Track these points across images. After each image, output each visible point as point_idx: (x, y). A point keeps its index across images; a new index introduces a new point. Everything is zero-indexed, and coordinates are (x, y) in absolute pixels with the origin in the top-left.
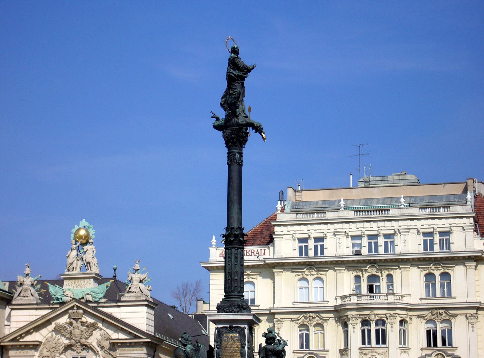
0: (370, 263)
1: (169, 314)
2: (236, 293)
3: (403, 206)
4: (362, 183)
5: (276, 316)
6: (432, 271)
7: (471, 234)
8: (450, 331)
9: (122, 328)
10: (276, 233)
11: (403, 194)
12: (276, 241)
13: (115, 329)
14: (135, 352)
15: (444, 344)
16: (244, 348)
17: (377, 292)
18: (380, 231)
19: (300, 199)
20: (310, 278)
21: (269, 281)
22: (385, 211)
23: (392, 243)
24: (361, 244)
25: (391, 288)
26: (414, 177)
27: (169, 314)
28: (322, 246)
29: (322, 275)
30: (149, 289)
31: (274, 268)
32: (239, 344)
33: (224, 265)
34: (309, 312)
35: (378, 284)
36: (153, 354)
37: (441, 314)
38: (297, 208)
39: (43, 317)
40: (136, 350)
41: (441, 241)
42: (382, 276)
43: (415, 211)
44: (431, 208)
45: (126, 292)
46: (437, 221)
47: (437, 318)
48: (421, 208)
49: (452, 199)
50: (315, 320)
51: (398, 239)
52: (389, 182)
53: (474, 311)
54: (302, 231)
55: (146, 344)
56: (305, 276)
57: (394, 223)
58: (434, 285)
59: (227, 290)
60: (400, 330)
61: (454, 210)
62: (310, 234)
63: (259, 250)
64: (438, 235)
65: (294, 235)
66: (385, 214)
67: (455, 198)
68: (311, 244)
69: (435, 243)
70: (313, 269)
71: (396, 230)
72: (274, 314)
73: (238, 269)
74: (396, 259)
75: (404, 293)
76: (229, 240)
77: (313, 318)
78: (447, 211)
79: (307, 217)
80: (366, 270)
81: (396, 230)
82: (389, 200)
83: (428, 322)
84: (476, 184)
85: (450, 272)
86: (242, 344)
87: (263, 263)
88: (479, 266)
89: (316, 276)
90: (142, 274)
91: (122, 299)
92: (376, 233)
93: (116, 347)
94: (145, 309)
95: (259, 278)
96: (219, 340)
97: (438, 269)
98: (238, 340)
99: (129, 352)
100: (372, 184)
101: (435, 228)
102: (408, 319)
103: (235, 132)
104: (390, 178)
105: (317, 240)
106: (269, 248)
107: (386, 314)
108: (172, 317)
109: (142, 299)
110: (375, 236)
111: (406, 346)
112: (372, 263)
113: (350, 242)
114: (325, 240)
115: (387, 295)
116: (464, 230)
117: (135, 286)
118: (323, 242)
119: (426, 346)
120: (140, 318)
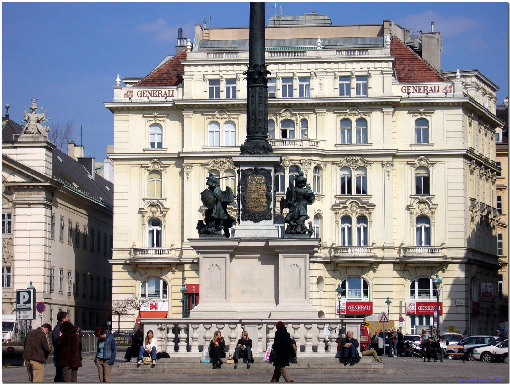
0: (285, 108)
1: (58, 157)
2: (260, 134)
3: (319, 48)
4: (272, 23)
5: (185, 161)
6: (348, 117)
7: (389, 78)
8: (365, 179)
9: (19, 171)
10: (185, 73)
11: (320, 35)
12: (186, 82)
13: (12, 172)
14: (33, 196)
15: (358, 191)
16: (270, 191)
17: (291, 138)
18: (295, 73)
19: (207, 38)
20: (221, 122)
21: (177, 124)
22: (301, 52)
23: (308, 86)
24: (275, 87)
25: (306, 133)
26: (326, 18)
27: (58, 157)
29: (233, 118)
30: (47, 130)
31: (183, 110)
32: (265, 186)
33: (246, 103)
34: (220, 157)
35: (292, 129)
36: (51, 198)
37: (357, 161)
38: (205, 47)
40: (34, 194)
41: (358, 85)
42: (296, 121)
43: (332, 54)
44: (346, 50)
45: (22, 132)
46: (356, 65)
47: (352, 165)
48: (339, 51)
49: (368, 41)
50: (226, 165)
51: (313, 83)
52: (301, 22)
53: (390, 159)
54: (213, 72)
55: (45, 188)
56: (216, 119)
57: (310, 66)
58: (350, 131)
59: (250, 130)
60: (315, 176)
61: (372, 53)
62: (222, 75)
63: (433, 86)
64: (355, 79)
65: (205, 75)
66: (301, 55)
67: (371, 41)
68: (223, 86)
69: (294, 88)
70: (225, 112)
71: (313, 73)
72: (183, 158)
73: (262, 108)
74: (312, 104)
75: (319, 138)
76: (252, 77)
77: (224, 163)
78: (366, 54)
79: (216, 57)
80: (280, 114)
81: (313, 73)
82: (302, 41)
83: (343, 169)
84: (393, 27)
85: (367, 118)
86: (268, 188)
87: (171, 105)
88: (396, 112)
89: (227, 120)
90: (39, 113)
91: (19, 140)
92: (291, 75)
93: (12, 190)
94: (43, 151)
95: (167, 120)
96: (243, 183)
97: (354, 115)
98: (264, 183)
99: (27, 196)
100: (283, 24)
101: (353, 72)
102: (322, 166)
104: (301, 18)
105: (229, 81)
106: (177, 89)
107: (300, 160)
108: (61, 160)
109: (40, 140)
110: (290, 79)
111: (320, 193)
112: (287, 107)
114: (238, 82)
115: (302, 141)
116: (383, 74)
117: (32, 126)
118: (236, 84)
119: (340, 194)
120: (37, 160)
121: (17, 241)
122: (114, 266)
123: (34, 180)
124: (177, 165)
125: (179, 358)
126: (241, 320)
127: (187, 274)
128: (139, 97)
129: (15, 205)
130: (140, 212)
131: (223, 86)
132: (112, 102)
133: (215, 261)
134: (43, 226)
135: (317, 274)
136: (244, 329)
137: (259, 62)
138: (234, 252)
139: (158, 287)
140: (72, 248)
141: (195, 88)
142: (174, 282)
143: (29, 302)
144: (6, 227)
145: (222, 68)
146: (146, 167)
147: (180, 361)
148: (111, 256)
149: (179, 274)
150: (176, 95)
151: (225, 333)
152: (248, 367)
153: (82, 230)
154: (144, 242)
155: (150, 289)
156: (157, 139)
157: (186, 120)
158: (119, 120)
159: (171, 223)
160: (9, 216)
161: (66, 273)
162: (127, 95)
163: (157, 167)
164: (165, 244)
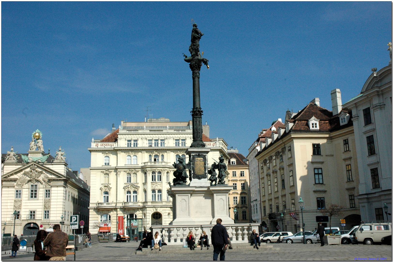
11: (168, 125)
12: (119, 141)
20: (132, 155)
21: (115, 156)
23: (164, 143)
28: (137, 143)
32: (203, 163)
38: (124, 128)
39: (19, 168)
51: (166, 142)
54: (129, 137)
68: (132, 142)
72: (117, 169)
75: (168, 161)
94: (64, 166)
100: (153, 121)
103: (196, 64)
110: (157, 140)
113: (147, 142)
117: (59, 157)
121: (52, 201)
122: (294, 140)
123: (60, 177)
124: (115, 171)
125: (172, 245)
126: (201, 226)
127: (118, 213)
128: (101, 146)
129: (51, 187)
130: (101, 189)
131: (132, 142)
132: (90, 148)
133: (183, 197)
134: (62, 195)
135: (168, 212)
136: (202, 230)
137: (198, 106)
138: (192, 193)
139: (107, 217)
140: (72, 203)
141: (122, 143)
142: (113, 215)
143: (76, 221)
144: (48, 195)
145: (132, 136)
146: (103, 172)
147: (172, 247)
148: (89, 206)
149: (115, 212)
150: (114, 145)
151: (194, 231)
152: (208, 249)
153: (76, 197)
154: (102, 201)
155: (104, 218)
156: (107, 162)
157: (118, 155)
158: (93, 154)
159: (112, 193)
160: (49, 191)
161: (70, 213)
162: (96, 146)
163: (107, 172)
164: (110, 201)
